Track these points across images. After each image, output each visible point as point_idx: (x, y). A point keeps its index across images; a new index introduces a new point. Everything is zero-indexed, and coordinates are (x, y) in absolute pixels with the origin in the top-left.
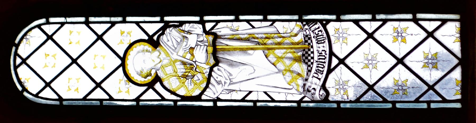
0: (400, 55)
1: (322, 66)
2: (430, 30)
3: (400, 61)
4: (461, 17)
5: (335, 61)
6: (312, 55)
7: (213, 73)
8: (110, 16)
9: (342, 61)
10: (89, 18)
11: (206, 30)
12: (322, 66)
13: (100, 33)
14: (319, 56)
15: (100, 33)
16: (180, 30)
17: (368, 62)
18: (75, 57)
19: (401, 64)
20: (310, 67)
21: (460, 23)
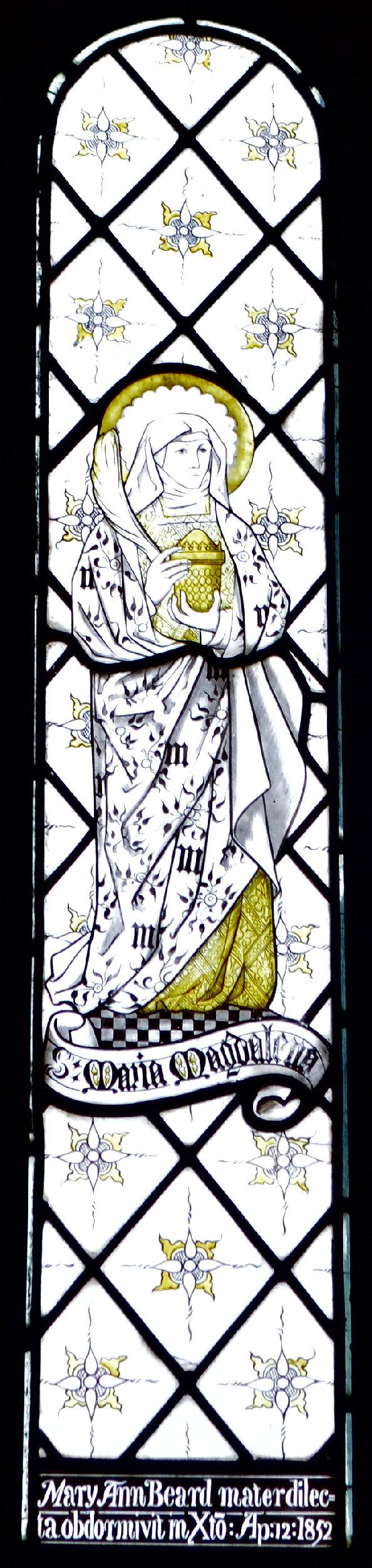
0: (267, 636)
1: (243, 1058)
2: (300, 1271)
3: (187, 139)
4: (336, 362)
5: (183, 351)
6: (154, 1036)
7: (232, 951)
8: (160, 1546)
9: (185, 326)
10: (66, 646)
11: (137, 1451)
12: (243, 1058)
13: (85, 228)
14: (156, 1085)
15: (85, 228)
16: (158, 1492)
17: (89, 513)
18: (171, 325)
19: (97, 216)
20: (238, 1012)
21: (292, 1270)
